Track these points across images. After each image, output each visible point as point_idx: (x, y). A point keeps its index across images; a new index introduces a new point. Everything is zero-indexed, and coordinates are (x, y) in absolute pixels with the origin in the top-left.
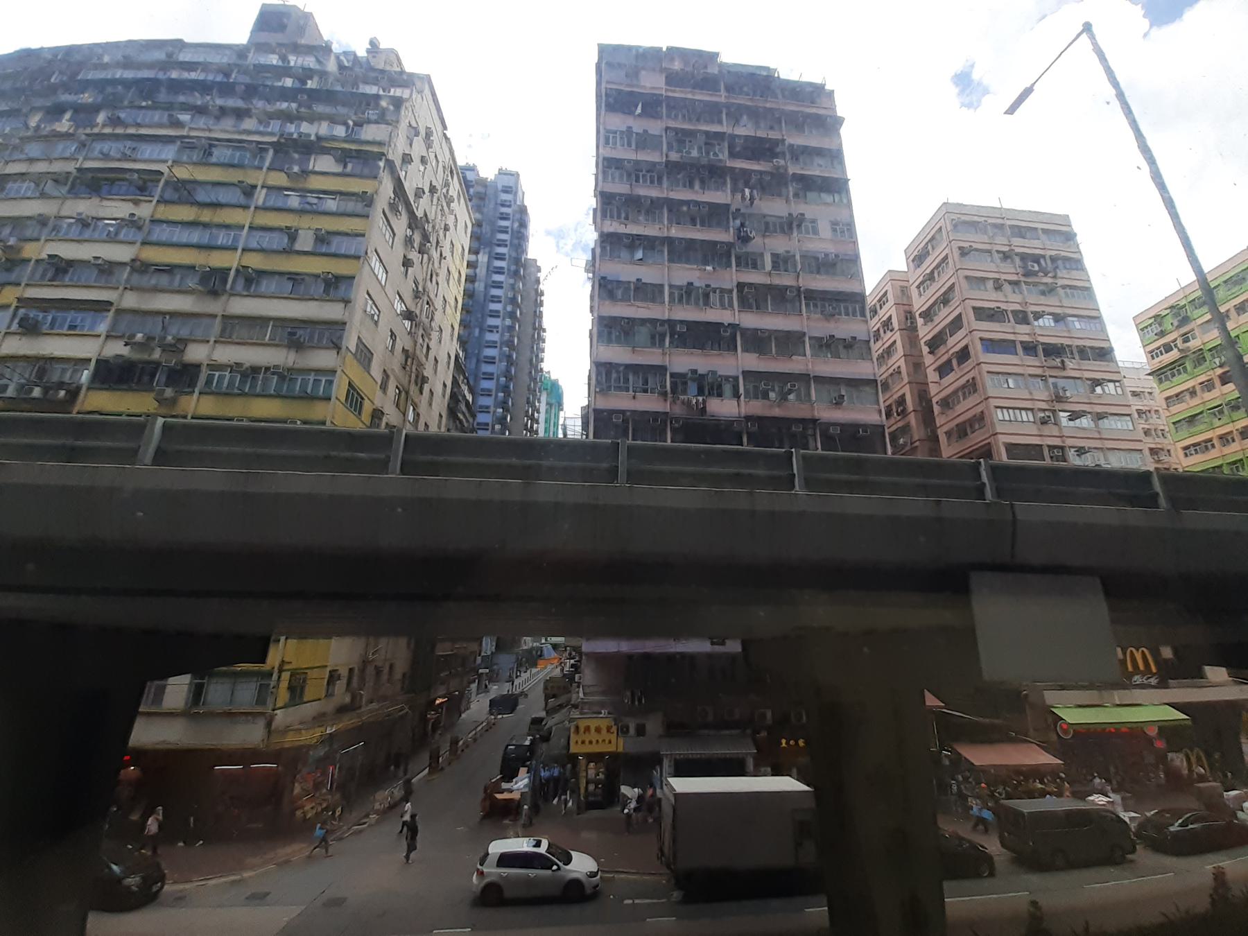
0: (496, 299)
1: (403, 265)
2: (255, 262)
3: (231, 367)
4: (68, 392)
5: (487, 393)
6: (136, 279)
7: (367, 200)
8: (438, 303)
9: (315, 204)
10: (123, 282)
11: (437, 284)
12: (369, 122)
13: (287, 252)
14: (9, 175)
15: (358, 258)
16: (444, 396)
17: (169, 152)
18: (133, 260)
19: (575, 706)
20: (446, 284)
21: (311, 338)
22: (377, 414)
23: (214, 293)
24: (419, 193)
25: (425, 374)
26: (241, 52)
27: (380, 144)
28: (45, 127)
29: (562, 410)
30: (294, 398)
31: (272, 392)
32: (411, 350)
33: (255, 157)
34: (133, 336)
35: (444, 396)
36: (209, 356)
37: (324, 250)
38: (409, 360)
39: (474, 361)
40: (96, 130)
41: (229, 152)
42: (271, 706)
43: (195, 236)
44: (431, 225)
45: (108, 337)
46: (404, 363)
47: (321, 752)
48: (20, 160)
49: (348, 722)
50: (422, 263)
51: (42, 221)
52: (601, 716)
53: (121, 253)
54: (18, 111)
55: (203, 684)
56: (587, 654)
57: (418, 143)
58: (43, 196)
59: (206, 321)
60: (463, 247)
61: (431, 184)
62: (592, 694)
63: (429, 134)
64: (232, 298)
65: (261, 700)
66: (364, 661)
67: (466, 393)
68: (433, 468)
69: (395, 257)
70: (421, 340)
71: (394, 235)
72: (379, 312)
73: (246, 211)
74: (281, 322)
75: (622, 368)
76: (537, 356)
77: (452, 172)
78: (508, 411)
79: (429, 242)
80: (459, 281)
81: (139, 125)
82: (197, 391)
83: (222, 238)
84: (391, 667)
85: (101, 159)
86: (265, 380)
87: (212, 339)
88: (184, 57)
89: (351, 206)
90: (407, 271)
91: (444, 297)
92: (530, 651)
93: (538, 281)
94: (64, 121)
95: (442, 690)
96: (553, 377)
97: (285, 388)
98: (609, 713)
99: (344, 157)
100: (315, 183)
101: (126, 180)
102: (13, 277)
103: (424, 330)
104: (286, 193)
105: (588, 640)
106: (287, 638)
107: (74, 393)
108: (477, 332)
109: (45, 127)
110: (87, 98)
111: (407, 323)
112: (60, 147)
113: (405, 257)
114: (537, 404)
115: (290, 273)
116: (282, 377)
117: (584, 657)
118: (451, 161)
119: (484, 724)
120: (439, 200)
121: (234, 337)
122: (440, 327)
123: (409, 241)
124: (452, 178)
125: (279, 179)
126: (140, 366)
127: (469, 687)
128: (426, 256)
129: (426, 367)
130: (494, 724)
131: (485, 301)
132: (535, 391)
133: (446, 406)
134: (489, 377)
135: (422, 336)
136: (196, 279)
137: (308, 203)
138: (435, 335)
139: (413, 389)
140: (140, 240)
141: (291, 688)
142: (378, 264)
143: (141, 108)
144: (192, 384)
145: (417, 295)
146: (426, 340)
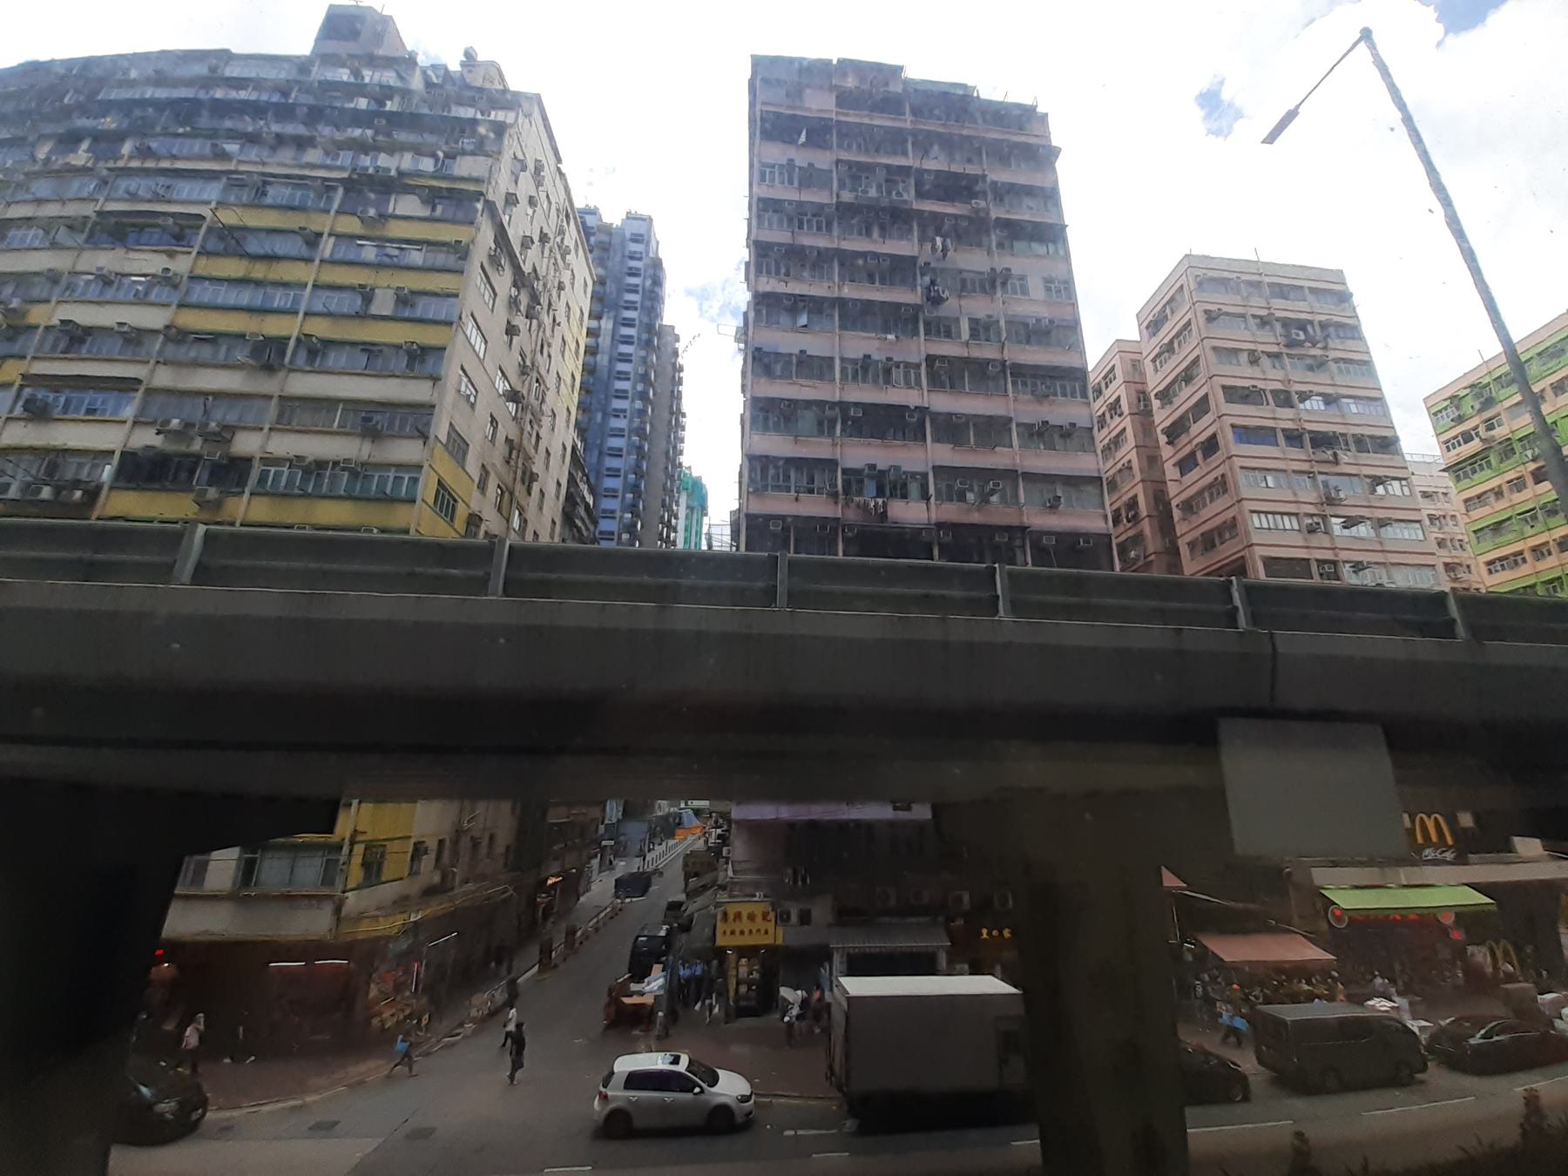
0: (623, 376)
1: (507, 334)
2: (320, 329)
3: (290, 461)
4: (85, 492)
5: (612, 494)
6: (171, 351)
7: (461, 251)
8: (551, 381)
9: (396, 256)
10: (155, 354)
11: (550, 356)
12: (464, 153)
13: (361, 317)
14: (12, 220)
15: (450, 324)
16: (558, 498)
17: (213, 191)
18: (167, 327)
19: (723, 888)
20: (560, 357)
22: (474, 520)
23: (269, 369)
24: (526, 242)
25: (535, 470)
26: (303, 65)
27: (478, 181)
28: (57, 160)
29: (706, 515)
30: (369, 500)
31: (342, 492)
32: (516, 440)
33: (320, 197)
34: (168, 422)
35: (558, 498)
36: (262, 447)
37: (407, 314)
38: (514, 452)
39: (596, 453)
40: (120, 164)
41: (288, 191)
42: (340, 888)
43: (245, 297)
44: (541, 283)
45: (135, 423)
46: (507, 456)
47: (404, 945)
48: (25, 201)
49: (437, 907)
50: (530, 330)
51: (53, 277)
52: (755, 899)
53: (152, 318)
54: (23, 139)
55: (255, 859)
56: (738, 822)
57: (526, 180)
58: (54, 246)
59: (259, 403)
60: (581, 311)
61: (541, 232)
62: (743, 872)
63: (539, 168)
64: (292, 375)
65: (328, 880)
66: (457, 831)
67: (586, 493)
68: (544, 588)
69: (496, 322)
70: (528, 428)
71: (495, 295)
72: (477, 392)
73: (309, 265)
74: (353, 404)
75: (781, 463)
76: (675, 447)
77: (567, 216)
78: (638, 516)
79: (539, 304)
80: (577, 353)
81: (174, 157)
82: (247, 491)
83: (279, 299)
84: (492, 837)
85: (127, 200)
86: (333, 477)
87: (267, 426)
88: (232, 71)
89: (441, 259)
90: (511, 340)
91: (558, 373)
92: (666, 818)
93: (676, 353)
94: (80, 152)
95: (555, 867)
96: (695, 474)
97: (358, 487)
98: (765, 896)
99: (432, 197)
100: (396, 230)
101: (158, 226)
102: (16, 348)
103: (532, 414)
104: (359, 242)
105: (738, 804)
106: (360, 802)
107: (93, 494)
108: (599, 417)
109: (57, 160)
110: (109, 123)
111: (512, 406)
112: (76, 184)
113: (508, 322)
114: (675, 508)
115: (364, 343)
116: (354, 474)
117: (733, 826)
118: (567, 203)
119: (609, 910)
120: (551, 251)
121: (294, 423)
122: (553, 411)
123: (513, 303)
124: (568, 223)
125: (350, 225)
126: (176, 459)
127: (589, 863)
128: (535, 322)
129: (536, 461)
130: (620, 910)
131: (609, 378)
132: (673, 491)
133: (560, 510)
134: (614, 473)
135: (531, 422)
137: (387, 255)
138: (546, 421)
139: (519, 489)
140: (176, 302)
141: (366, 865)
142: (474, 331)
143: (178, 135)
144: (242, 482)
145: (524, 371)
146: (536, 427)
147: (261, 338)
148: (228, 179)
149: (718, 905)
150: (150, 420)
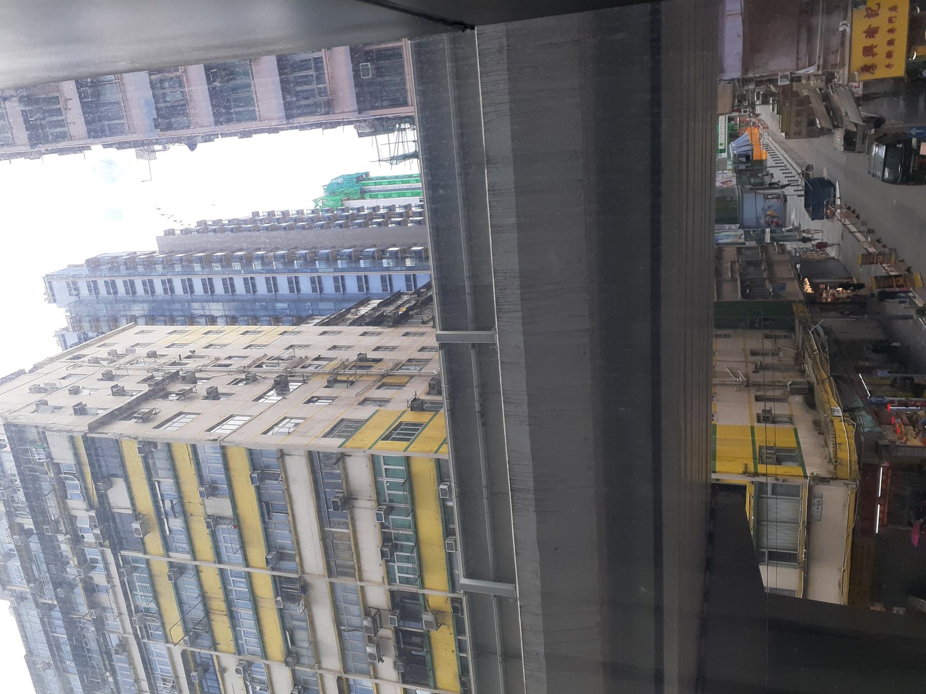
0: (229, 285)
1: (219, 399)
2: (258, 554)
3: (387, 561)
5: (363, 282)
7: (147, 448)
8: (255, 354)
9: (172, 502)
10: (314, 671)
11: (230, 358)
12: (49, 456)
15: (223, 448)
16: (379, 334)
17: (157, 648)
18: (287, 664)
19: (830, 78)
20: (226, 348)
21: (339, 486)
22: (417, 405)
23: (305, 588)
24: (118, 392)
25: (355, 358)
27: (72, 439)
29: (367, 174)
31: (410, 518)
32: (327, 377)
33: (136, 569)
35: (379, 334)
36: (379, 585)
38: (339, 378)
39: (322, 306)
41: (139, 593)
43: (245, 613)
44: (155, 374)
45: (376, 678)
46: (345, 385)
47: (867, 420)
49: (828, 396)
50: (208, 379)
52: (848, 30)
55: (770, 553)
56: (745, 70)
57: (53, 400)
59: (340, 594)
60: (170, 333)
61: (102, 380)
62: (811, 53)
63: (38, 389)
64: (307, 570)
65: (792, 492)
66: (747, 386)
67: (370, 307)
68: (480, 291)
69: (212, 410)
70: (311, 369)
71: (180, 414)
72: (285, 418)
73: (201, 569)
74: (323, 520)
75: (289, 98)
76: (296, 220)
77: (78, 357)
78: (383, 252)
79: (178, 372)
80: (218, 332)
81: (137, 680)
82: (421, 591)
83: (239, 587)
84: (754, 353)
86: (397, 526)
87: (359, 583)
89: (160, 462)
92: (739, 173)
93: (186, 232)
95: (793, 287)
96: (321, 193)
97: (403, 506)
98: (845, 19)
99: (103, 478)
100: (145, 503)
103: (295, 367)
104: (168, 533)
105: (722, 70)
106: (715, 472)
108: (280, 305)
111: (293, 386)
113: (206, 398)
114: (366, 212)
116: (390, 510)
117: (750, 75)
119: (847, 222)
120: (119, 368)
121: (352, 563)
123: (183, 396)
124: (84, 356)
125: (153, 541)
126: (403, 646)
127: (790, 252)
128: (198, 375)
129: (344, 359)
130: (849, 208)
131: (234, 301)
132: (347, 217)
133: (392, 329)
134: (340, 283)
135: (303, 367)
136: (292, 606)
137: (172, 507)
138: (299, 353)
140: (264, 661)
141: (779, 461)
143: (116, 682)
144: (414, 596)
145: (251, 379)
146: (309, 362)
147: (279, 598)
148: (143, 638)
149: (851, 78)
150: (371, 669)
